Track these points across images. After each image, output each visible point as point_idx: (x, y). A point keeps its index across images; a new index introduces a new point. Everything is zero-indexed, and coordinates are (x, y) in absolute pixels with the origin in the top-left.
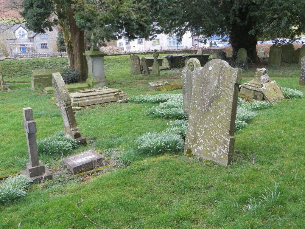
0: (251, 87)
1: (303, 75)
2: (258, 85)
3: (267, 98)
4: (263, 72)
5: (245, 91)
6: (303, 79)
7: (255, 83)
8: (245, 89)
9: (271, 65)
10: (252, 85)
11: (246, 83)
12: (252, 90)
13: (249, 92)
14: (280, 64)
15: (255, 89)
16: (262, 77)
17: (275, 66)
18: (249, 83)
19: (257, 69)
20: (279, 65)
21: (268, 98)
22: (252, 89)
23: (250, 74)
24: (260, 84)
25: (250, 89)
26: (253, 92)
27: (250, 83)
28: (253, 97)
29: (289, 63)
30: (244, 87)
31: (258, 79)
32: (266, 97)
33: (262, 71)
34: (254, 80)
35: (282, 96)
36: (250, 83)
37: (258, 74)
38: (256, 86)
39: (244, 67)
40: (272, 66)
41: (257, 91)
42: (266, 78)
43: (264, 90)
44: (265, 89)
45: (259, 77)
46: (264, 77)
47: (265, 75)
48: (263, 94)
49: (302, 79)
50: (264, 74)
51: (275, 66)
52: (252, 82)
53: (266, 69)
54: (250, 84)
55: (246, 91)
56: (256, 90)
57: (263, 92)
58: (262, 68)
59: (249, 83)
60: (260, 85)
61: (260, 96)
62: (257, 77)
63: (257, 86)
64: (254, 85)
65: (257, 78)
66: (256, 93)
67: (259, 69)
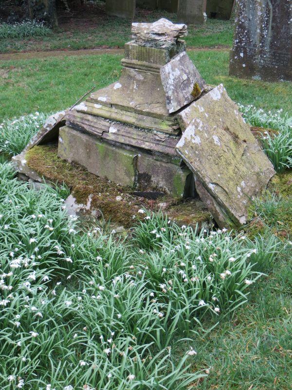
0: (113, 130)
1: (240, 42)
2: (149, 114)
3: (215, 197)
4: (167, 42)
5: (81, 151)
6: (242, 55)
7: (132, 104)
8: (84, 137)
9: (115, 14)
10: (115, 113)
11: (82, 106)
12: (122, 146)
13: (106, 156)
14: (134, 11)
15: (135, 139)
16: (168, 68)
17: (124, 16)
18: (97, 102)
19: (133, 24)
20: (134, 15)
21: (222, 197)
22: (122, 140)
23: (68, 40)
24: (158, 110)
25: (110, 137)
26: (127, 155)
27: (104, 104)
28: (128, 180)
29: (149, 9)
30: (74, 126)
31: (143, 82)
32: (208, 190)
33: (162, 38)
34: (125, 87)
35: (265, 165)
36: (104, 104)
37: (143, 55)
38: (142, 124)
39: (48, 21)
40: (117, 17)
41: (149, 152)
42: (185, 77)
43: (194, 148)
44: (197, 140)
45: (149, 68)
46: (177, 72)
47: (177, 58)
48: (184, 165)
49: (239, 56)
50: (172, 54)
51: (124, 16)
52: (115, 100)
53: (180, 26)
54: (104, 111)
55: (88, 147)
56: (146, 146)
57: (195, 165)
58: (155, 19)
59: (97, 102)
60: (160, 117)
61: (170, 176)
62: (140, 69)
63: (147, 122)
64: (130, 118)
65: (140, 77)
66: (145, 162)
67: (144, 25)
